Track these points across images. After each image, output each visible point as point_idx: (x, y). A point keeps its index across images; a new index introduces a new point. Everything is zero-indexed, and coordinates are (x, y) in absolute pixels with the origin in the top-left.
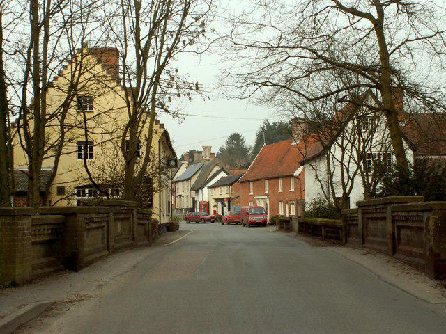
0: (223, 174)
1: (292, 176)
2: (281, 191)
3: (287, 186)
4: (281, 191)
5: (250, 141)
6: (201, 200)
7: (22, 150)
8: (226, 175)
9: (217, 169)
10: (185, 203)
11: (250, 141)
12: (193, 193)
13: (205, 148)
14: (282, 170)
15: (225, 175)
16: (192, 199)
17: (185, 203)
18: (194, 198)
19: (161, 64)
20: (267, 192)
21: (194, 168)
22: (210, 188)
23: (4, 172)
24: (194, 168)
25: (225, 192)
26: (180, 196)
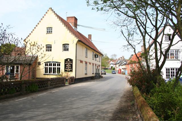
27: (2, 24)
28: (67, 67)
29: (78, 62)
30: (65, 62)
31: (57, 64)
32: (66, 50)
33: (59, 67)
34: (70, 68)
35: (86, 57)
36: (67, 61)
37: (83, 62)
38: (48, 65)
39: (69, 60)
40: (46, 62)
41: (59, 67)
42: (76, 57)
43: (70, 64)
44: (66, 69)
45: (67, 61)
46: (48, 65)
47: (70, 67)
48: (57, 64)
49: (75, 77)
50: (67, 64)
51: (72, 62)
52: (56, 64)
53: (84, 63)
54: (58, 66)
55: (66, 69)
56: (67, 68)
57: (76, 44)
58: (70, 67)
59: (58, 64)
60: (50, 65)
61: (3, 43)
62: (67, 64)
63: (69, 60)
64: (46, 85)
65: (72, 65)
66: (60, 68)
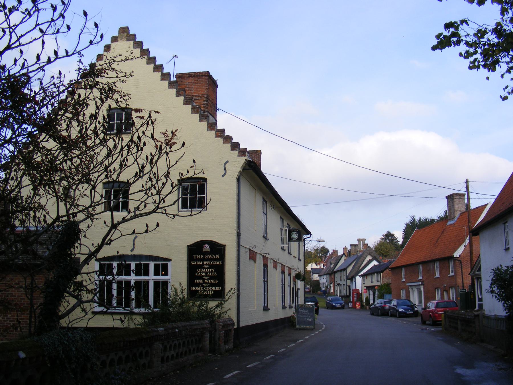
0: (375, 263)
1: (451, 258)
2: (437, 276)
3: (444, 270)
4: (437, 276)
5: (399, 237)
6: (354, 288)
7: (30, 19)
8: (377, 264)
9: (369, 258)
10: (342, 291)
11: (399, 237)
12: (349, 281)
13: (359, 240)
14: (438, 253)
15: (377, 264)
16: (348, 288)
17: (342, 291)
18: (349, 287)
19: (334, 270)
20: (420, 278)
21: (351, 259)
22: (362, 276)
23: (1, 75)
24: (351, 259)
25: (375, 281)
26: (338, 284)
27: (85, 14)
28: (201, 278)
29: (245, 255)
30: (191, 258)
31: (152, 265)
32: (193, 206)
33: (161, 278)
34: (212, 285)
35: (415, 216)
36: (200, 252)
37: (258, 256)
38: (133, 267)
39: (207, 248)
40: (105, 259)
41: (161, 278)
42: (239, 235)
43: (211, 266)
44: (193, 288)
45: (200, 252)
46: (133, 267)
47: (211, 278)
48: (152, 265)
49: (235, 320)
50: (201, 266)
51: (222, 258)
52: (147, 266)
53: (260, 260)
54: (156, 273)
55: (193, 288)
56: (198, 285)
57: (238, 180)
58: (211, 278)
59: (156, 267)
60: (125, 270)
61: (84, 120)
62: (201, 266)
63: (207, 248)
64: (500, 301)
65: (220, 271)
66: (165, 283)
